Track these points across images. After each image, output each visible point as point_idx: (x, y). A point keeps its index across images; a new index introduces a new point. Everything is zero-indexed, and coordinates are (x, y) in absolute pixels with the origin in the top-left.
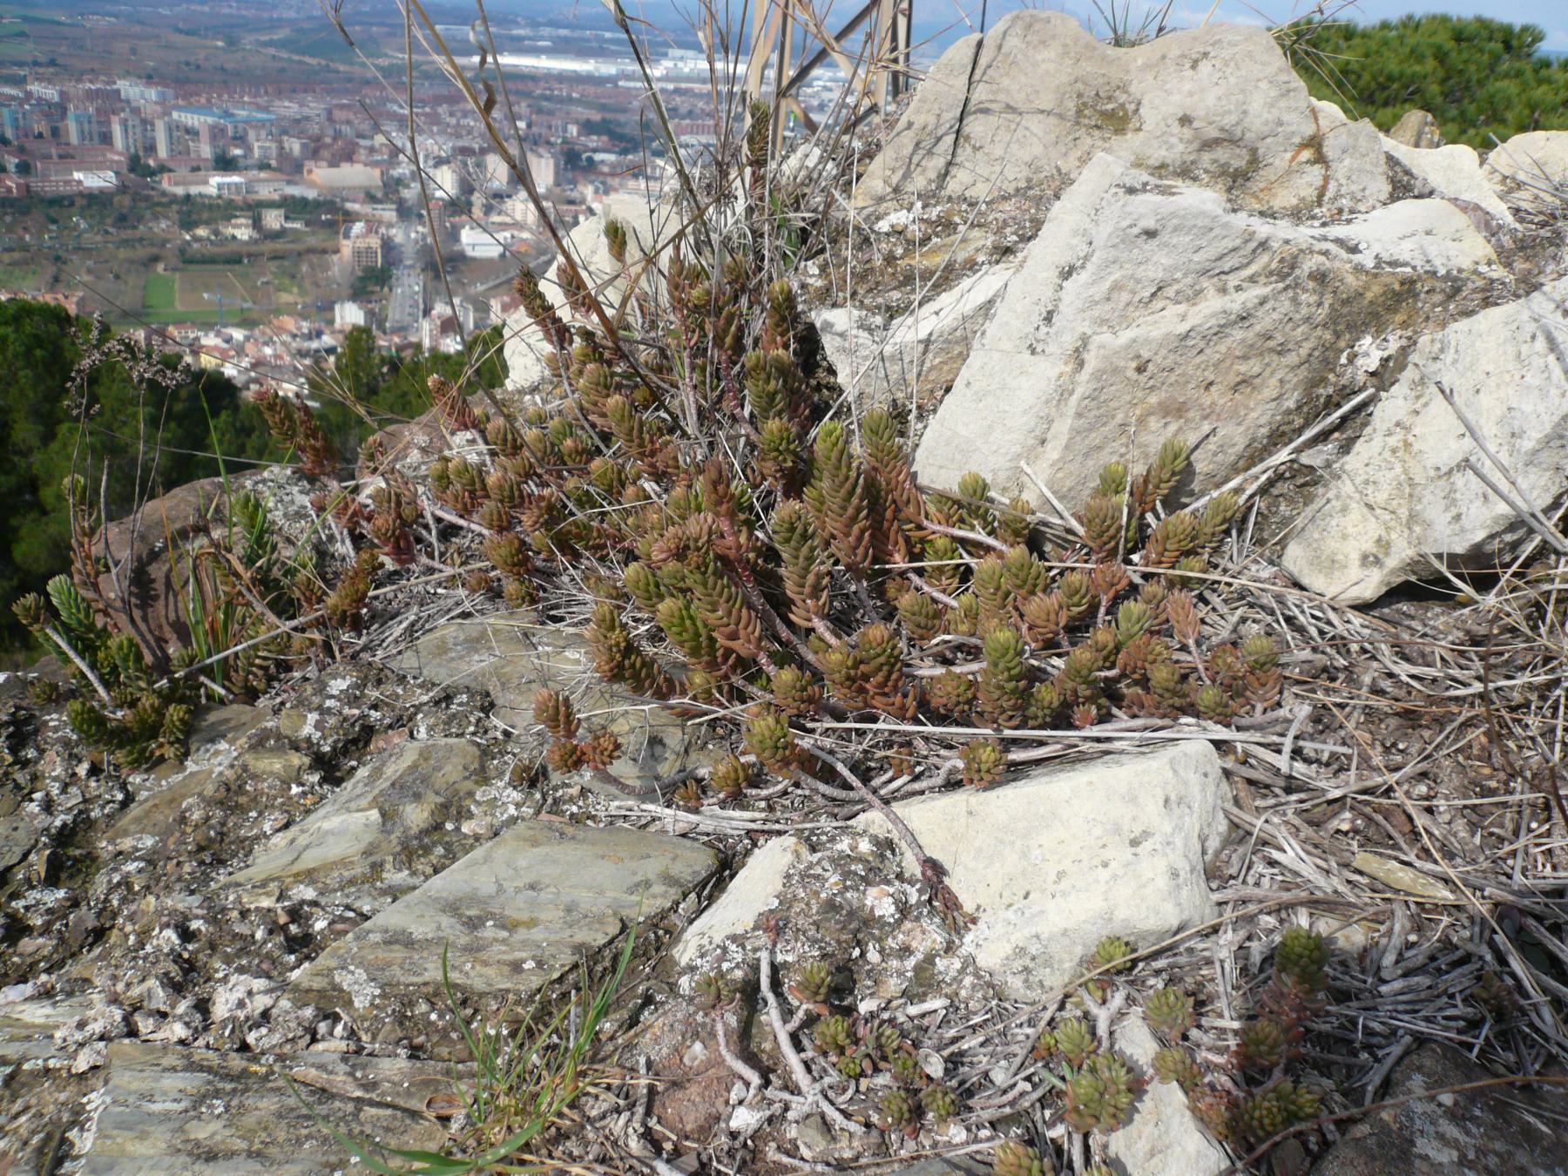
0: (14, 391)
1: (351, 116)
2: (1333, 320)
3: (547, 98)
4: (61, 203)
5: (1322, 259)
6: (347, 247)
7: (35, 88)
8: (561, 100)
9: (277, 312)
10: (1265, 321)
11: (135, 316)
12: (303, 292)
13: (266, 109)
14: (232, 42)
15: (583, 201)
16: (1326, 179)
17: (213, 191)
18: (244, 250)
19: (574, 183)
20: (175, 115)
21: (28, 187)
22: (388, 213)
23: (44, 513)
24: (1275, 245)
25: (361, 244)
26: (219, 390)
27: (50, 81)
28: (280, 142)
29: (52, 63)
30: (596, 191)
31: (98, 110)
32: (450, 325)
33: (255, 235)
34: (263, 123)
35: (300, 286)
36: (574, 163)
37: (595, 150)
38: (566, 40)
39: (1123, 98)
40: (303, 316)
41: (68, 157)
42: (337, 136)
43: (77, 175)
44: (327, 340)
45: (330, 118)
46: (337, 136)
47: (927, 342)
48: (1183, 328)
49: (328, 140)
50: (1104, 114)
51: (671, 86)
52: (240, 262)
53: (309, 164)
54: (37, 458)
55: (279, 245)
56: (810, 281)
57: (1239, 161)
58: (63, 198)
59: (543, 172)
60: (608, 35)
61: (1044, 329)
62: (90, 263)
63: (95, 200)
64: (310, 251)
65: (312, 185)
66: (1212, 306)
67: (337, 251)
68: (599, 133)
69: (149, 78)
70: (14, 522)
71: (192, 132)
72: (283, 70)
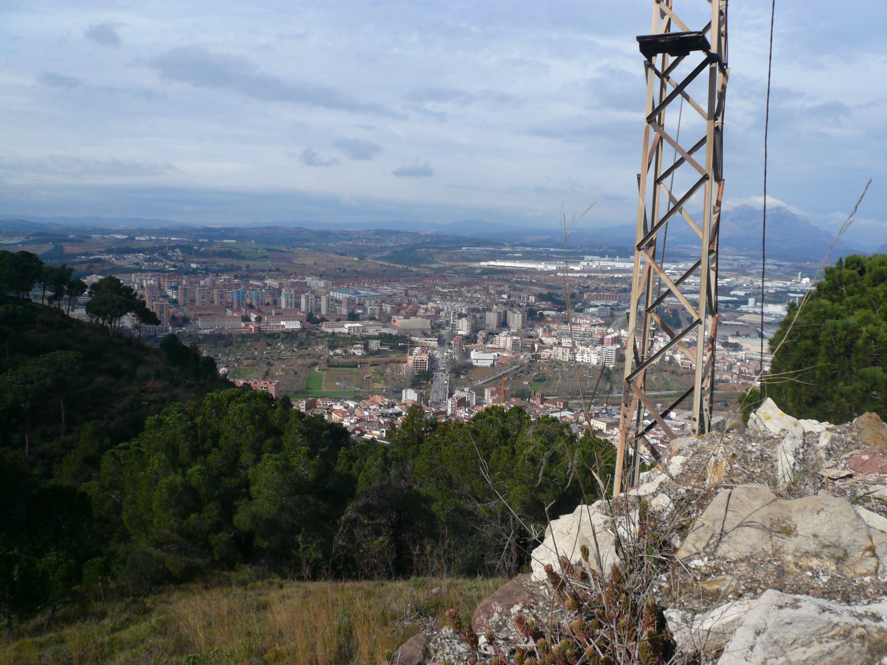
0: (243, 436)
1: (417, 293)
2: (870, 650)
3: (518, 283)
4: (274, 337)
5: (863, 630)
6: (410, 360)
7: (268, 282)
8: (526, 283)
9: (373, 393)
10: (840, 653)
11: (302, 393)
12: (386, 383)
13: (375, 291)
14: (361, 258)
15: (537, 336)
16: (878, 564)
17: (346, 331)
18: (359, 360)
19: (532, 326)
20: (331, 294)
21: (259, 328)
22: (433, 343)
23: (251, 499)
24: (841, 625)
25: (418, 358)
26: (339, 433)
27: (275, 278)
28: (381, 306)
29: (278, 270)
30: (544, 331)
31: (296, 292)
32: (462, 403)
33: (365, 353)
34: (373, 297)
35: (385, 380)
36: (533, 316)
37: (544, 310)
38: (530, 252)
39: (789, 522)
40: (386, 395)
41: (280, 315)
42: (410, 302)
43: (282, 323)
44: (397, 409)
45: (406, 295)
46: (410, 302)
47: (709, 631)
48: (805, 657)
49: (405, 305)
50: (782, 527)
51: (586, 275)
52: (356, 367)
53: (395, 317)
54: (251, 471)
55: (376, 359)
56: (663, 584)
57: (840, 554)
58: (275, 334)
59: (516, 319)
60: (552, 250)
61: (750, 653)
62: (283, 366)
63: (290, 335)
64: (391, 362)
65: (395, 328)
66: (815, 650)
67: (406, 362)
68: (546, 300)
69: (321, 276)
70: (236, 503)
71: (338, 302)
72: (385, 271)
